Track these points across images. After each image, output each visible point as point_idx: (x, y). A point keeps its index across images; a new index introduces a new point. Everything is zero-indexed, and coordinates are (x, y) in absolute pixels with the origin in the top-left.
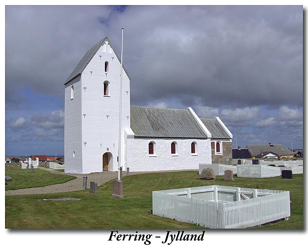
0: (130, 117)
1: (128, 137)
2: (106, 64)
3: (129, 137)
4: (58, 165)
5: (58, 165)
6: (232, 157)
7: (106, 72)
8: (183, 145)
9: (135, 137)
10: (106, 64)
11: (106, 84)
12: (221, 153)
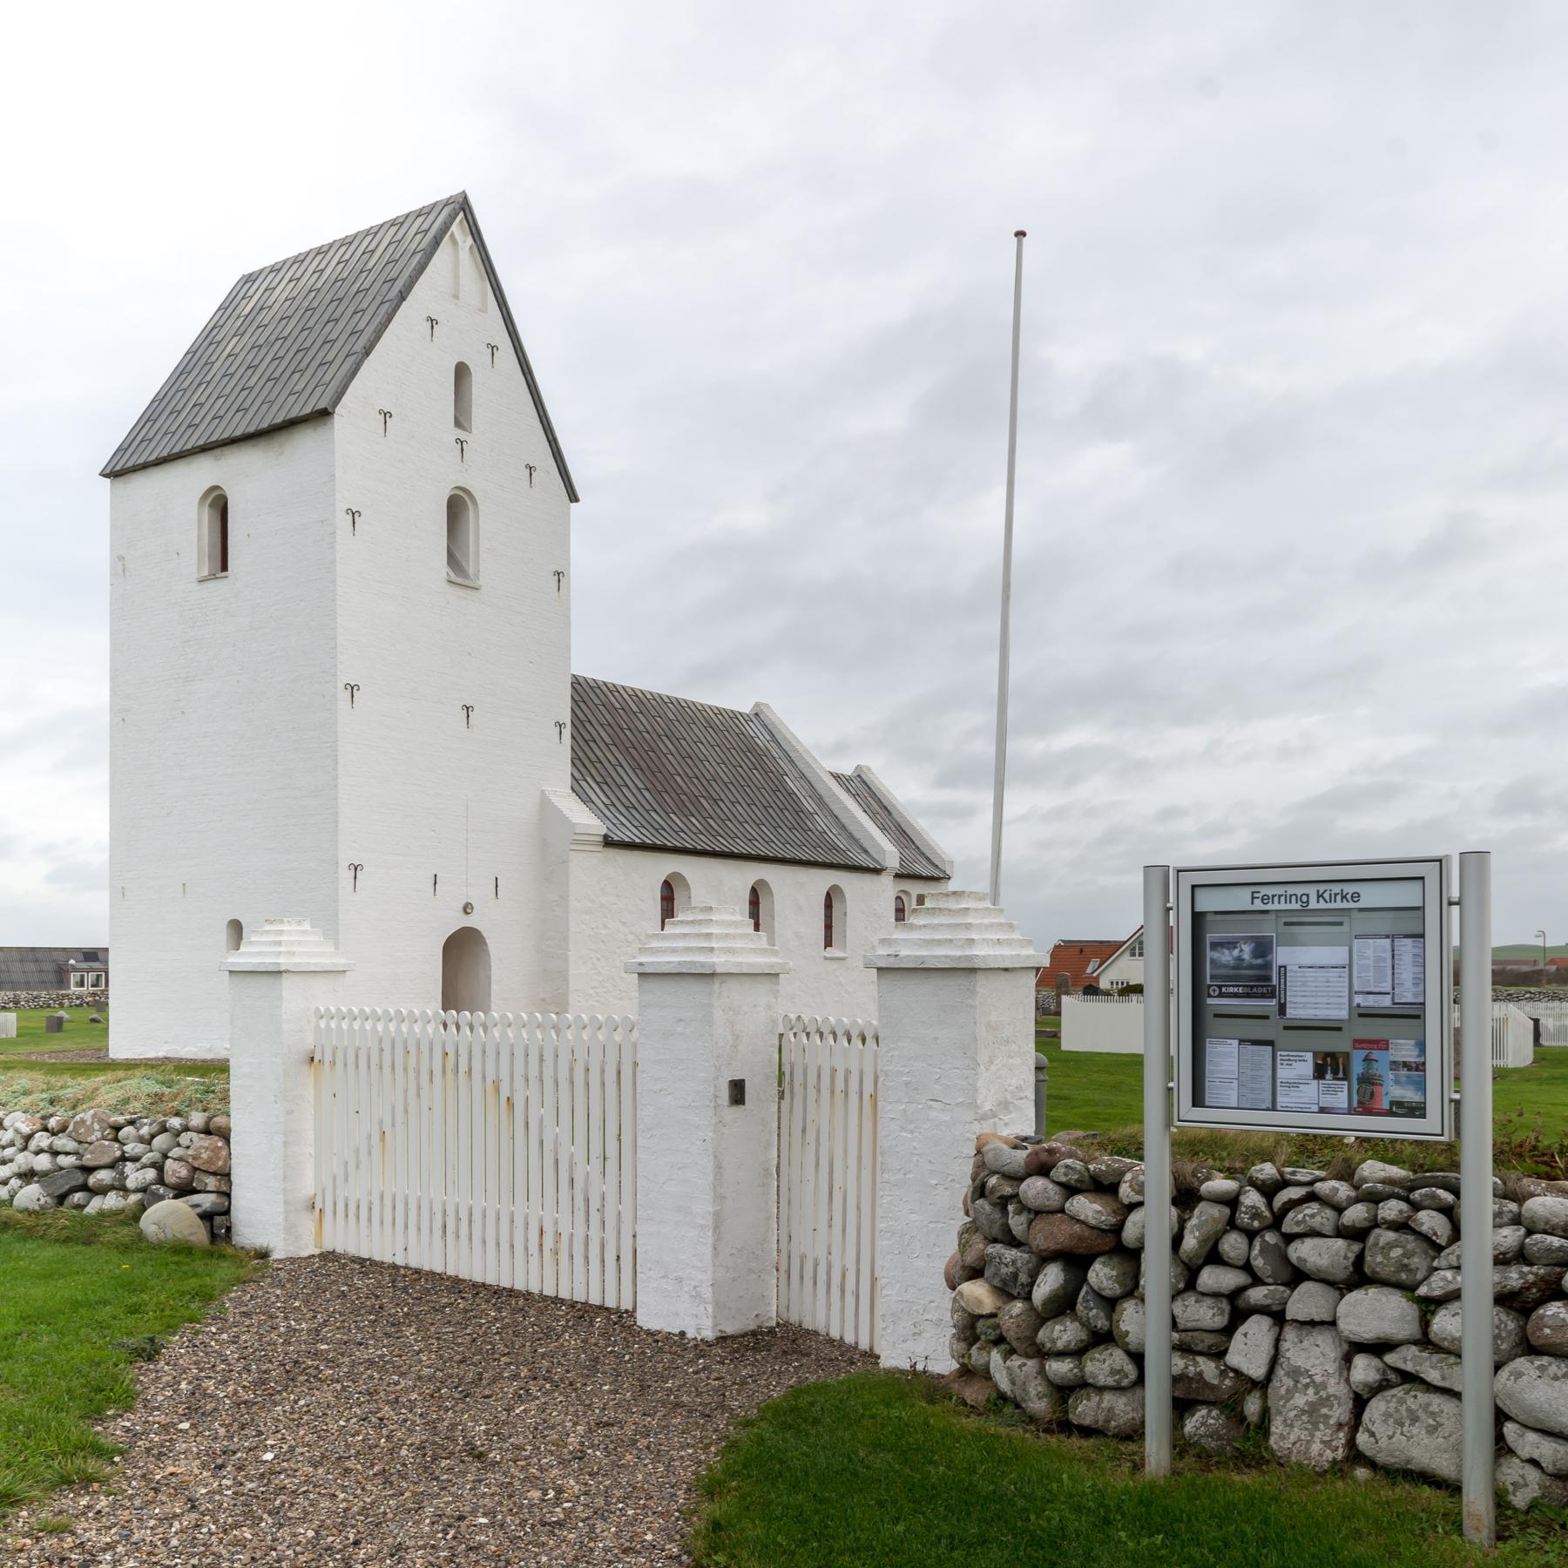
0: (569, 724)
1: (576, 842)
2: (461, 372)
3: (579, 841)
7: (462, 435)
8: (797, 893)
9: (609, 843)
10: (461, 372)
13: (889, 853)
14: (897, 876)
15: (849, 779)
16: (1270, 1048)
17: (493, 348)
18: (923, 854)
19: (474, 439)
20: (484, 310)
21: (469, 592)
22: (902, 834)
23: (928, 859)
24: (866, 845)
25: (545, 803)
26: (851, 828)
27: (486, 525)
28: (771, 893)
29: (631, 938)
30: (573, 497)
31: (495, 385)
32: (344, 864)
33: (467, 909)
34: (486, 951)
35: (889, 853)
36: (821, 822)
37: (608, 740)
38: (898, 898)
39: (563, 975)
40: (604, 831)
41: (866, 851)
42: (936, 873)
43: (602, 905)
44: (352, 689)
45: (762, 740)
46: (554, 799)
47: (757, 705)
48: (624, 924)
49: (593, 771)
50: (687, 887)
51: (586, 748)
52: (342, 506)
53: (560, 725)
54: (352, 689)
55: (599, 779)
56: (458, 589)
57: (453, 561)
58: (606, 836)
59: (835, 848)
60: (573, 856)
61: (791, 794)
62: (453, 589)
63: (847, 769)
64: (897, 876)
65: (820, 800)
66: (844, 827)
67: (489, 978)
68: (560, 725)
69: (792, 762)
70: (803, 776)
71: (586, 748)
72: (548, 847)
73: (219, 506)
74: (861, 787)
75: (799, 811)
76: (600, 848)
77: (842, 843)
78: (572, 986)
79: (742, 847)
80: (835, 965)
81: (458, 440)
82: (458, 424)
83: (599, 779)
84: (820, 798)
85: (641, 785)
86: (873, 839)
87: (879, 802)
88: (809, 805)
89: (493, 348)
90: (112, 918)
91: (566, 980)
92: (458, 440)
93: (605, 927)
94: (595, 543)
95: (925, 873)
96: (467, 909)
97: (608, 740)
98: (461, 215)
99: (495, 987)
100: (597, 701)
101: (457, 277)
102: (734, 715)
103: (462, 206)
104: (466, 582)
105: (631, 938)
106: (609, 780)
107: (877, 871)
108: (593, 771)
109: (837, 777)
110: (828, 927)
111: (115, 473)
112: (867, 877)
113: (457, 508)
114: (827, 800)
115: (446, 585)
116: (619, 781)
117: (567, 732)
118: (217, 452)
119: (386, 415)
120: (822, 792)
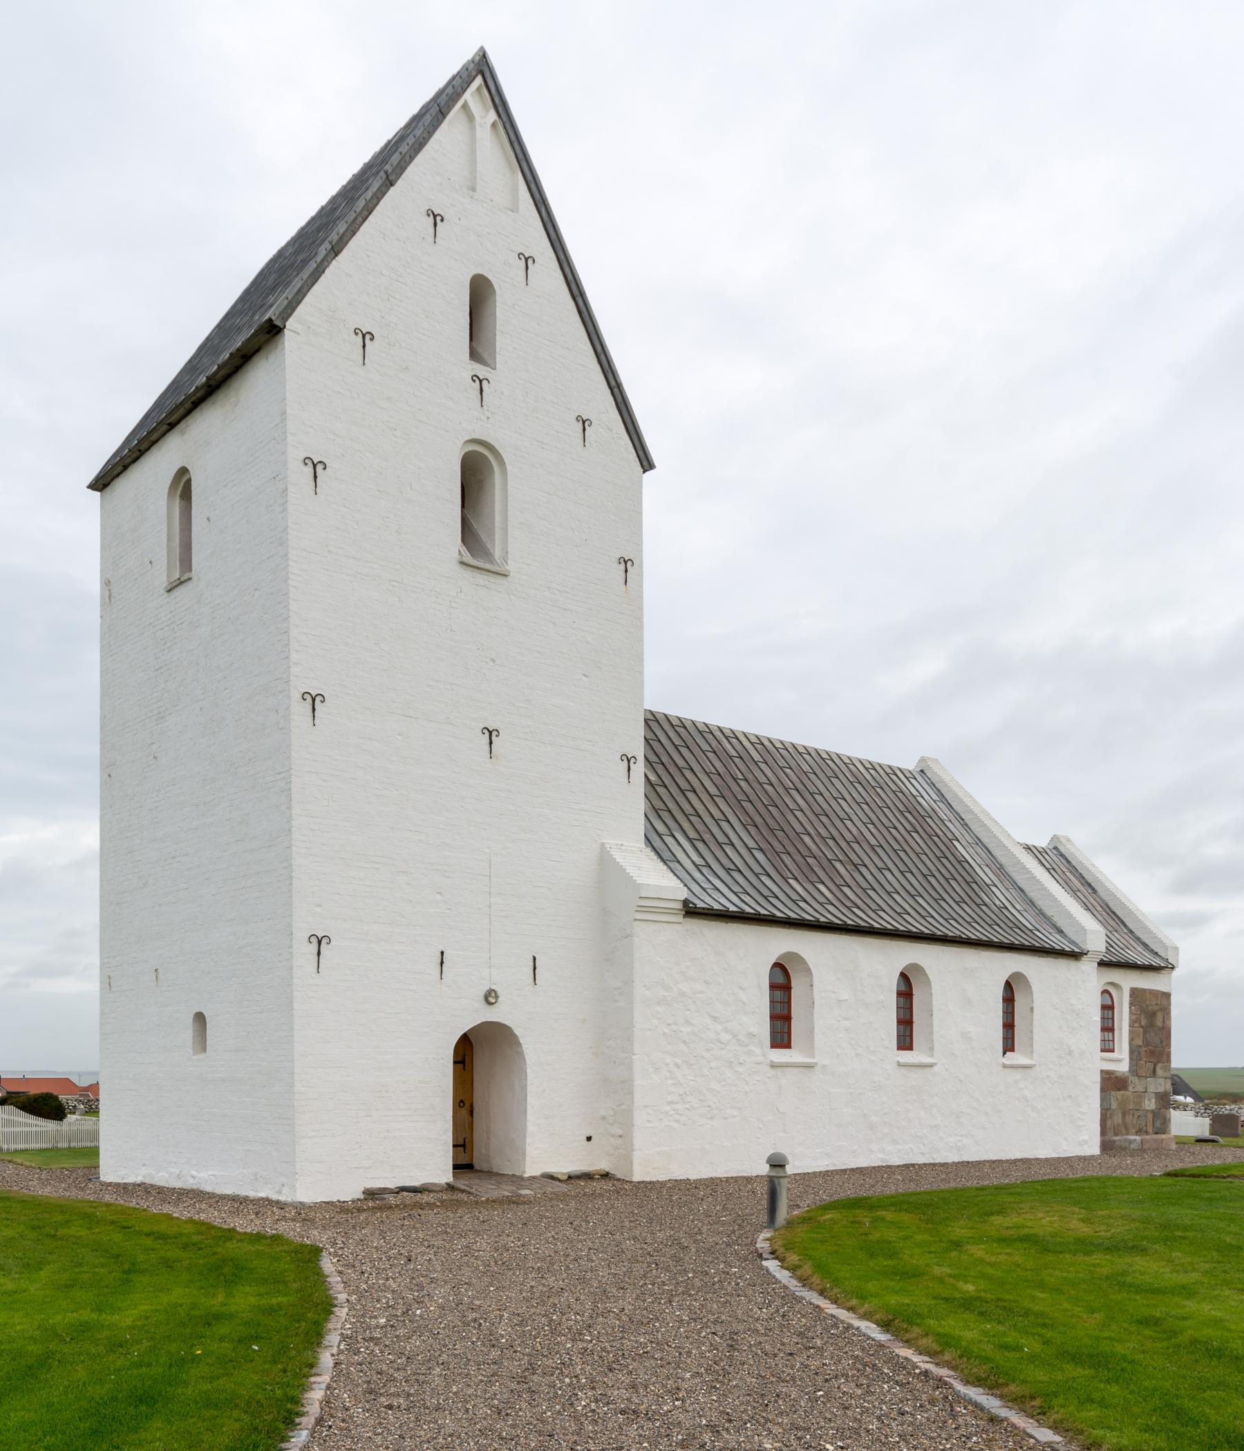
0: (641, 759)
1: (642, 909)
2: (480, 294)
3: (648, 908)
4: (26, 1125)
5: (26, 1125)
6: (66, 1145)
7: (482, 371)
8: (962, 986)
9: (691, 911)
10: (480, 294)
11: (475, 475)
12: (1120, 1061)
13: (1094, 935)
14: (1102, 964)
15: (1043, 852)
16: (435, 1167)
17: (527, 260)
18: (1138, 939)
19: (501, 377)
20: (514, 209)
21: (492, 578)
22: (1111, 914)
23: (1145, 945)
24: (1061, 923)
25: (604, 859)
26: (1040, 903)
27: (516, 497)
28: (928, 983)
29: (725, 1037)
30: (647, 464)
31: (530, 306)
32: (301, 935)
33: (490, 997)
34: (521, 1055)
35: (1094, 935)
36: (1001, 895)
37: (713, 790)
38: (1105, 992)
39: (624, 1088)
40: (683, 894)
41: (1060, 932)
42: (1156, 962)
43: (683, 994)
44: (314, 700)
45: (927, 800)
46: (618, 856)
47: (923, 760)
48: (715, 1019)
49: (686, 825)
50: (808, 971)
51: (681, 799)
52: (295, 455)
53: (629, 760)
54: (314, 700)
55: (692, 834)
56: (476, 574)
57: (468, 533)
58: (686, 902)
59: (1018, 926)
60: (639, 928)
61: (962, 862)
62: (468, 574)
63: (1042, 842)
64: (1102, 964)
65: (1001, 870)
66: (1032, 903)
67: (524, 1089)
68: (629, 760)
69: (965, 825)
70: (979, 841)
71: (681, 799)
72: (609, 914)
73: (182, 486)
74: (1058, 859)
75: (971, 882)
76: (680, 918)
77: (1028, 920)
78: (638, 1101)
79: (886, 921)
80: (1017, 1075)
81: (475, 378)
82: (474, 355)
83: (692, 834)
84: (1001, 867)
85: (751, 844)
86: (1070, 916)
87: (1081, 878)
88: (985, 875)
89: (527, 260)
90: (102, 1014)
91: (631, 1093)
92: (475, 378)
93: (688, 1022)
94: (677, 522)
95: (1140, 960)
96: (490, 997)
97: (713, 790)
98: (479, 81)
99: (532, 1101)
100: (705, 747)
101: (473, 162)
102: (892, 772)
103: (481, 68)
104: (488, 566)
105: (725, 1037)
106: (707, 837)
107: (1075, 956)
108: (686, 825)
109: (1028, 848)
110: (1009, 1026)
111: (101, 483)
112: (1062, 964)
113: (475, 475)
114: (1010, 870)
115: (458, 568)
116: (721, 838)
117: (639, 769)
118: (182, 425)
119: (366, 336)
120: (1003, 860)
